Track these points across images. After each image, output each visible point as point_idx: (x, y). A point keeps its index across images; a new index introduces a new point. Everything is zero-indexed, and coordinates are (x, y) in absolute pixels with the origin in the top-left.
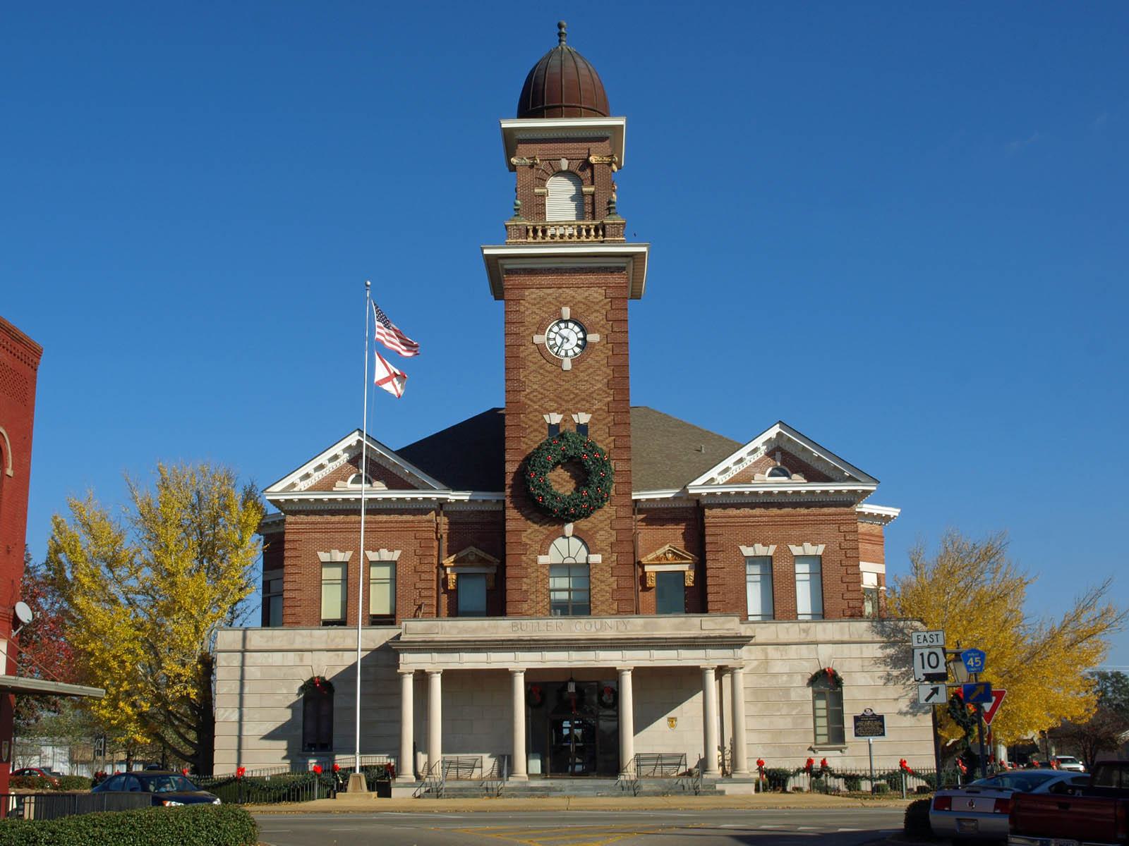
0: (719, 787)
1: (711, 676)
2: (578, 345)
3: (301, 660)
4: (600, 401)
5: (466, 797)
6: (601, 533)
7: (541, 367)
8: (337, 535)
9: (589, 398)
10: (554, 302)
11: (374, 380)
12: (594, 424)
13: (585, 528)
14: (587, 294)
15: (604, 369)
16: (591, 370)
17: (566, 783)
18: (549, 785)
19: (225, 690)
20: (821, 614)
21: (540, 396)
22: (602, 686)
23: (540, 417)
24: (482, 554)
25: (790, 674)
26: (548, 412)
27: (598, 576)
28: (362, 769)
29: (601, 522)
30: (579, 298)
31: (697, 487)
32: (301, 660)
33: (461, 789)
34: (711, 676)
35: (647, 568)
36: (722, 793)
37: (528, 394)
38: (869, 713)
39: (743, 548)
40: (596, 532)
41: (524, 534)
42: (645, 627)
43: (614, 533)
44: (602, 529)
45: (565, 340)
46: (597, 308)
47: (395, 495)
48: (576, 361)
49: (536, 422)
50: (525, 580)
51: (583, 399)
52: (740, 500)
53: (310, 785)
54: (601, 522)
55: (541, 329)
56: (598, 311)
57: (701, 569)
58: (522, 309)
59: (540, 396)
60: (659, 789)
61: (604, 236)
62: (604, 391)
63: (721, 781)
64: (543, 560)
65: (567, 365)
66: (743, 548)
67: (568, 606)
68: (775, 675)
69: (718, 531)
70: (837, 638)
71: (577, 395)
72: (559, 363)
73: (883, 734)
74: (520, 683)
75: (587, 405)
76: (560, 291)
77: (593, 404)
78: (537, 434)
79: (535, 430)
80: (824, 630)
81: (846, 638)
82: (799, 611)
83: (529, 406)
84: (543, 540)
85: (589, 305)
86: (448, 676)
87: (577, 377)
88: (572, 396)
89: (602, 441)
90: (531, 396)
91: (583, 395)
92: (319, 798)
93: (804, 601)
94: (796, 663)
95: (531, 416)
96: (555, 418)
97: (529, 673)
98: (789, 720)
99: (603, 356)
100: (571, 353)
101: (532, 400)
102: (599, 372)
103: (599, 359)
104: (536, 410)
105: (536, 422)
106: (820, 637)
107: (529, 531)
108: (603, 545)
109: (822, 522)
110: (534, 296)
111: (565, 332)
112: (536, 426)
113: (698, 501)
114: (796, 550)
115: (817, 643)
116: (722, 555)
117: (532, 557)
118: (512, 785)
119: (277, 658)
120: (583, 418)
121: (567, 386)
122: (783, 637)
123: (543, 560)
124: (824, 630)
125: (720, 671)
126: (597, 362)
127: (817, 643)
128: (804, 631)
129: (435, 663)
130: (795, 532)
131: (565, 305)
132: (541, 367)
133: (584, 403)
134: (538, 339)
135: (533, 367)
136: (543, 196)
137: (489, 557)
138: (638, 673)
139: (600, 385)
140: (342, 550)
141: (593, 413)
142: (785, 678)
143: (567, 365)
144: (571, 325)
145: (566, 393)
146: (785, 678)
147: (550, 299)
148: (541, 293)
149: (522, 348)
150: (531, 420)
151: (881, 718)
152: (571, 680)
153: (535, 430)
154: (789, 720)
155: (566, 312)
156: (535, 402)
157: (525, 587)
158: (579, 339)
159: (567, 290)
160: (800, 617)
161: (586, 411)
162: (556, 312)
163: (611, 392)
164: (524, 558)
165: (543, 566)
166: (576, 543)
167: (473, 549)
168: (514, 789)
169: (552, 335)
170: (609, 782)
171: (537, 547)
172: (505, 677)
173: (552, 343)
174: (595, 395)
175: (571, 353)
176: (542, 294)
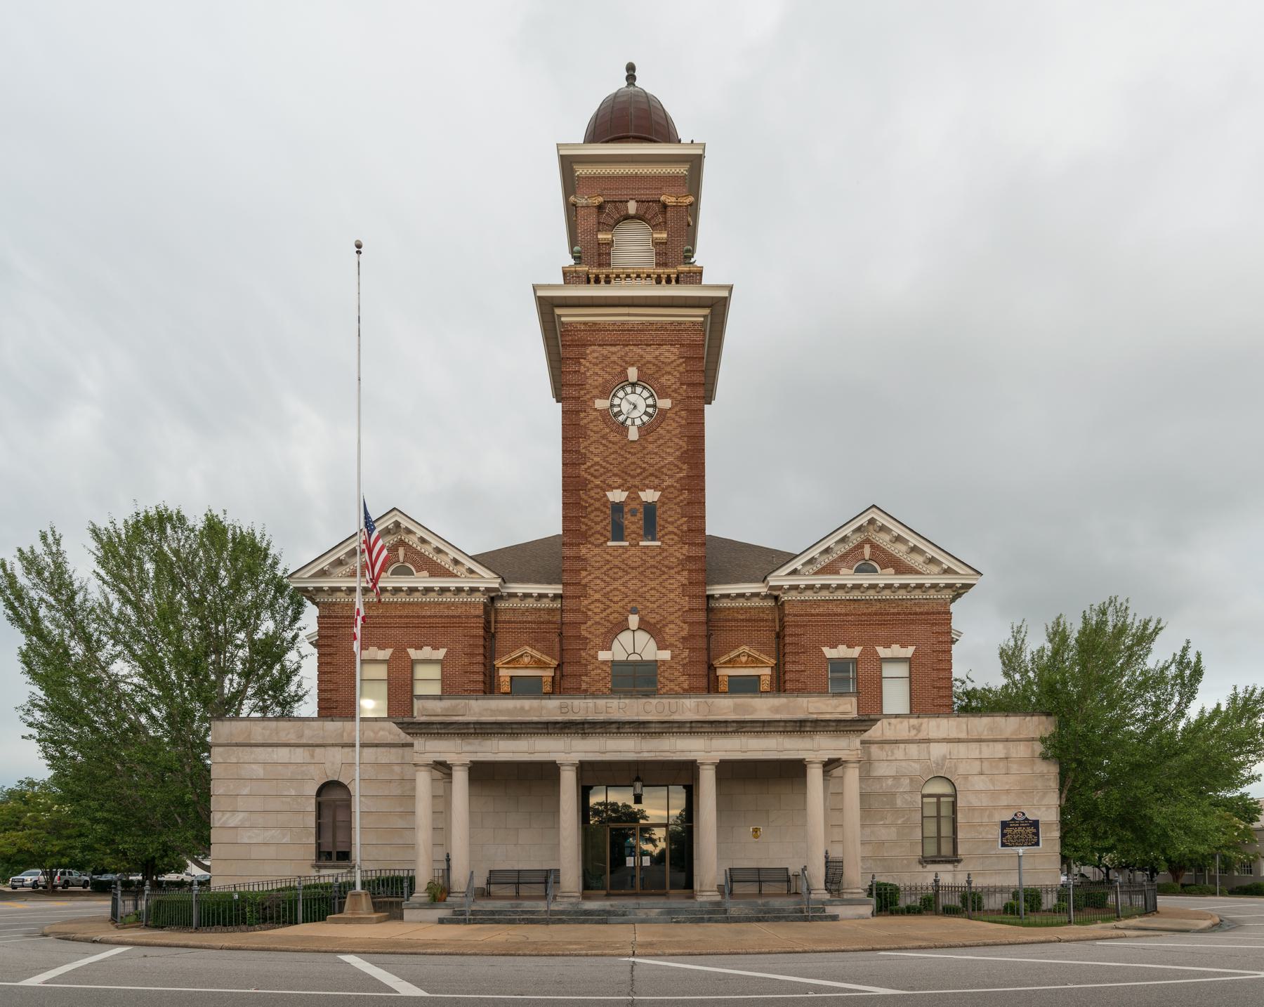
0: (830, 910)
2: (646, 413)
3: (312, 756)
4: (671, 477)
6: (672, 626)
7: (603, 437)
9: (658, 474)
10: (620, 362)
12: (664, 503)
13: (652, 621)
14: (657, 353)
15: (676, 440)
16: (661, 441)
17: (629, 903)
18: (608, 908)
19: (221, 791)
21: (602, 470)
23: (601, 494)
24: (537, 655)
26: (612, 488)
27: (666, 674)
28: (363, 884)
29: (672, 614)
30: (649, 358)
31: (773, 581)
32: (312, 756)
33: (493, 913)
34: (815, 776)
35: (720, 672)
36: (834, 918)
37: (589, 468)
38: (1021, 818)
40: (664, 626)
41: (583, 627)
42: (736, 708)
43: (685, 626)
44: (672, 622)
45: (634, 406)
46: (668, 369)
48: (645, 430)
50: (584, 678)
51: (652, 475)
53: (290, 908)
54: (672, 614)
55: (606, 391)
56: (669, 373)
58: (583, 369)
59: (602, 470)
60: (752, 914)
62: (676, 466)
63: (830, 903)
64: (603, 656)
65: (633, 434)
67: (643, 888)
68: (879, 778)
69: (799, 631)
70: (954, 735)
71: (644, 469)
72: (623, 428)
73: (1037, 844)
75: (657, 481)
77: (664, 481)
78: (598, 513)
79: (597, 509)
80: (938, 726)
81: (963, 735)
83: (590, 482)
84: (606, 633)
85: (659, 367)
87: (644, 448)
88: (639, 471)
90: (592, 470)
91: (651, 470)
92: (305, 920)
94: (904, 764)
95: (592, 493)
96: (617, 496)
98: (894, 829)
99: (675, 425)
100: (638, 422)
101: (592, 475)
102: (670, 444)
103: (672, 427)
104: (597, 486)
106: (933, 735)
107: (589, 623)
108: (672, 640)
109: (913, 622)
110: (595, 355)
111: (632, 398)
112: (597, 505)
114: (883, 652)
115: (928, 741)
116: (803, 656)
117: (592, 652)
118: (561, 908)
119: (282, 754)
120: (650, 496)
121: (633, 459)
123: (603, 656)
124: (938, 726)
125: (830, 765)
126: (668, 431)
127: (928, 741)
128: (914, 727)
129: (458, 752)
130: (883, 632)
131: (633, 365)
132: (603, 437)
133: (653, 478)
134: (601, 404)
135: (595, 437)
137: (546, 659)
139: (670, 459)
140: (381, 647)
141: (663, 490)
142: (890, 782)
143: (633, 434)
145: (633, 467)
146: (890, 782)
147: (614, 358)
149: (582, 415)
150: (591, 497)
151: (1035, 824)
153: (597, 509)
154: (894, 829)
155: (633, 373)
156: (596, 477)
158: (648, 406)
159: (635, 349)
161: (655, 488)
162: (621, 372)
163: (685, 467)
165: (605, 662)
166: (643, 637)
167: (529, 650)
168: (562, 912)
169: (617, 401)
170: (677, 902)
171: (598, 641)
172: (547, 773)
173: (616, 410)
174: (665, 470)
176: (605, 352)
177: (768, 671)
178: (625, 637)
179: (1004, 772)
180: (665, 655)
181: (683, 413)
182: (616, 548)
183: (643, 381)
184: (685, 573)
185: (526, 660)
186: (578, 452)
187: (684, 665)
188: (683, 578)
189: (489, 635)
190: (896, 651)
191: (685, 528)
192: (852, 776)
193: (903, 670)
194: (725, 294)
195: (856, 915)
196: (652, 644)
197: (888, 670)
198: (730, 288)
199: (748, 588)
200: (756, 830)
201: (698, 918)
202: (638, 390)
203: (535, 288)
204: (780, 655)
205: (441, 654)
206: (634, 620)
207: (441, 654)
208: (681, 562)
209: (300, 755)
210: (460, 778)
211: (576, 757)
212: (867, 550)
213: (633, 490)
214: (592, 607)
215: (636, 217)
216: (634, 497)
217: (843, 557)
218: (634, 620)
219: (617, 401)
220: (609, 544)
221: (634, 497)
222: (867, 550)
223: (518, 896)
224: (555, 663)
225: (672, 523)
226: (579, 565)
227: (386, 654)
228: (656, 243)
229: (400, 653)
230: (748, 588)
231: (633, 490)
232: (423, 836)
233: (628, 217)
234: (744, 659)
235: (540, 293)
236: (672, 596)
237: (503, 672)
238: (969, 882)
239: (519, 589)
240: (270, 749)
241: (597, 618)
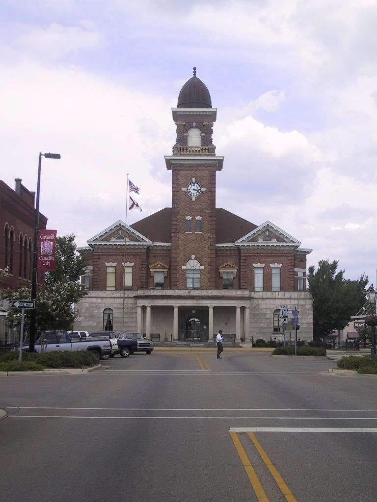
0: (241, 345)
1: (238, 311)
5: (159, 347)
8: (111, 257)
11: (12, 190)
12: (203, 221)
14: (202, 173)
20: (282, 289)
22: (202, 312)
25: (266, 309)
26: (187, 216)
31: (239, 243)
34: (238, 311)
35: (220, 271)
36: (241, 347)
39: (254, 265)
41: (178, 258)
43: (209, 259)
45: (193, 189)
47: (132, 243)
49: (183, 219)
52: (253, 247)
57: (148, 269)
61: (208, 152)
64: (184, 267)
65: (194, 199)
66: (254, 265)
68: (261, 309)
74: (176, 311)
76: (192, 172)
79: (182, 222)
82: (273, 286)
86: (153, 308)
89: (205, 226)
93: (276, 282)
95: (181, 217)
96: (189, 218)
97: (180, 308)
100: (195, 195)
105: (183, 219)
113: (239, 248)
114: (272, 266)
115: (276, 299)
120: (198, 218)
122: (102, 296)
123: (184, 267)
125: (243, 309)
127: (276, 299)
129: (147, 303)
131: (194, 177)
134: (184, 189)
136: (187, 136)
138: (215, 308)
139: (205, 206)
142: (265, 310)
143: (194, 199)
144: (196, 184)
146: (265, 310)
148: (186, 173)
152: (193, 309)
153: (182, 222)
157: (178, 277)
160: (108, 289)
164: (178, 267)
166: (196, 262)
167: (160, 263)
172: (171, 308)
173: (189, 191)
175: (195, 195)
177: (236, 271)
178: (191, 262)
179: (300, 305)
180: (203, 267)
181: (209, 192)
182: (188, 234)
183: (197, 182)
184: (209, 242)
185: (159, 266)
186: (177, 204)
187: (208, 271)
188: (208, 244)
189: (148, 256)
190: (276, 265)
191: (209, 228)
192: (247, 311)
193: (278, 271)
194: (222, 158)
195: (247, 346)
196: (199, 264)
197: (274, 271)
198: (224, 157)
199: (229, 245)
200: (226, 323)
201: (208, 346)
202: (196, 184)
203: (165, 156)
204: (240, 266)
205: (132, 264)
206: (193, 257)
207: (132, 264)
208: (208, 239)
209: (99, 300)
210: (148, 310)
211: (178, 305)
212: (267, 233)
213: (193, 216)
214: (181, 252)
215: (196, 127)
216: (193, 218)
217: (259, 235)
218: (193, 257)
219: (189, 188)
220: (186, 233)
221: (193, 218)
222: (267, 233)
223: (347, 350)
224: (168, 267)
225: (205, 226)
226: (177, 239)
227: (115, 264)
228: (202, 136)
229: (119, 264)
230: (229, 245)
231: (193, 216)
232: (139, 324)
233: (193, 127)
234: (228, 266)
235: (166, 158)
236: (205, 249)
237: (151, 270)
238: (275, 339)
239: (157, 244)
240: (90, 299)
241: (182, 256)
